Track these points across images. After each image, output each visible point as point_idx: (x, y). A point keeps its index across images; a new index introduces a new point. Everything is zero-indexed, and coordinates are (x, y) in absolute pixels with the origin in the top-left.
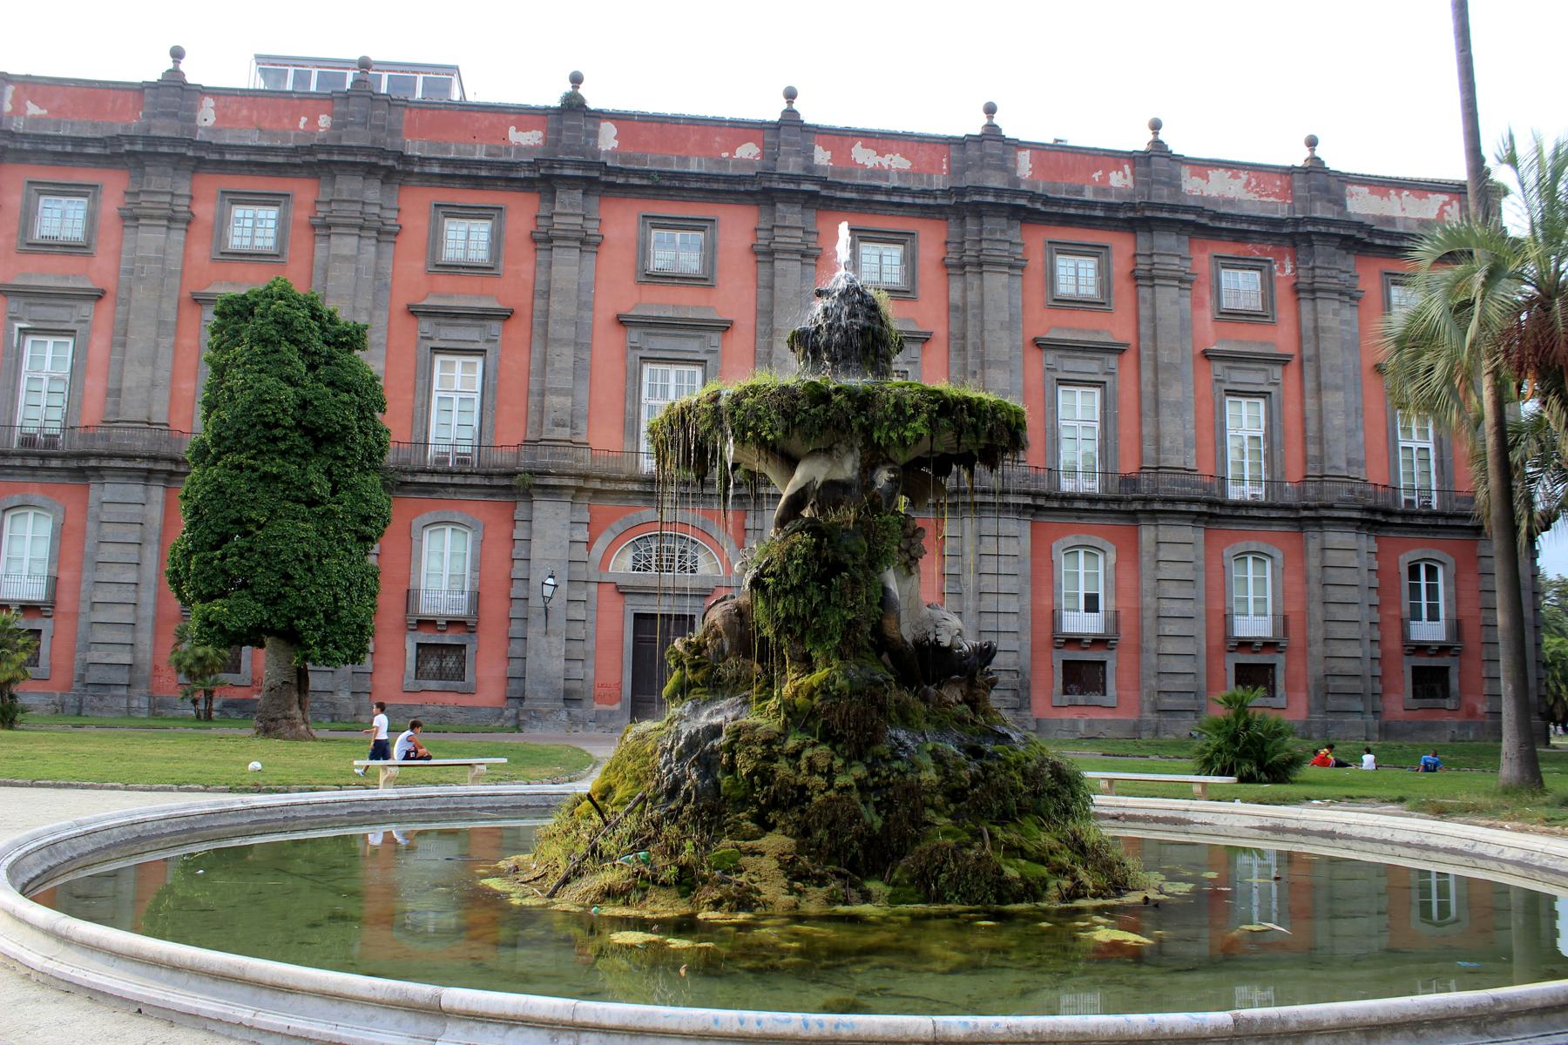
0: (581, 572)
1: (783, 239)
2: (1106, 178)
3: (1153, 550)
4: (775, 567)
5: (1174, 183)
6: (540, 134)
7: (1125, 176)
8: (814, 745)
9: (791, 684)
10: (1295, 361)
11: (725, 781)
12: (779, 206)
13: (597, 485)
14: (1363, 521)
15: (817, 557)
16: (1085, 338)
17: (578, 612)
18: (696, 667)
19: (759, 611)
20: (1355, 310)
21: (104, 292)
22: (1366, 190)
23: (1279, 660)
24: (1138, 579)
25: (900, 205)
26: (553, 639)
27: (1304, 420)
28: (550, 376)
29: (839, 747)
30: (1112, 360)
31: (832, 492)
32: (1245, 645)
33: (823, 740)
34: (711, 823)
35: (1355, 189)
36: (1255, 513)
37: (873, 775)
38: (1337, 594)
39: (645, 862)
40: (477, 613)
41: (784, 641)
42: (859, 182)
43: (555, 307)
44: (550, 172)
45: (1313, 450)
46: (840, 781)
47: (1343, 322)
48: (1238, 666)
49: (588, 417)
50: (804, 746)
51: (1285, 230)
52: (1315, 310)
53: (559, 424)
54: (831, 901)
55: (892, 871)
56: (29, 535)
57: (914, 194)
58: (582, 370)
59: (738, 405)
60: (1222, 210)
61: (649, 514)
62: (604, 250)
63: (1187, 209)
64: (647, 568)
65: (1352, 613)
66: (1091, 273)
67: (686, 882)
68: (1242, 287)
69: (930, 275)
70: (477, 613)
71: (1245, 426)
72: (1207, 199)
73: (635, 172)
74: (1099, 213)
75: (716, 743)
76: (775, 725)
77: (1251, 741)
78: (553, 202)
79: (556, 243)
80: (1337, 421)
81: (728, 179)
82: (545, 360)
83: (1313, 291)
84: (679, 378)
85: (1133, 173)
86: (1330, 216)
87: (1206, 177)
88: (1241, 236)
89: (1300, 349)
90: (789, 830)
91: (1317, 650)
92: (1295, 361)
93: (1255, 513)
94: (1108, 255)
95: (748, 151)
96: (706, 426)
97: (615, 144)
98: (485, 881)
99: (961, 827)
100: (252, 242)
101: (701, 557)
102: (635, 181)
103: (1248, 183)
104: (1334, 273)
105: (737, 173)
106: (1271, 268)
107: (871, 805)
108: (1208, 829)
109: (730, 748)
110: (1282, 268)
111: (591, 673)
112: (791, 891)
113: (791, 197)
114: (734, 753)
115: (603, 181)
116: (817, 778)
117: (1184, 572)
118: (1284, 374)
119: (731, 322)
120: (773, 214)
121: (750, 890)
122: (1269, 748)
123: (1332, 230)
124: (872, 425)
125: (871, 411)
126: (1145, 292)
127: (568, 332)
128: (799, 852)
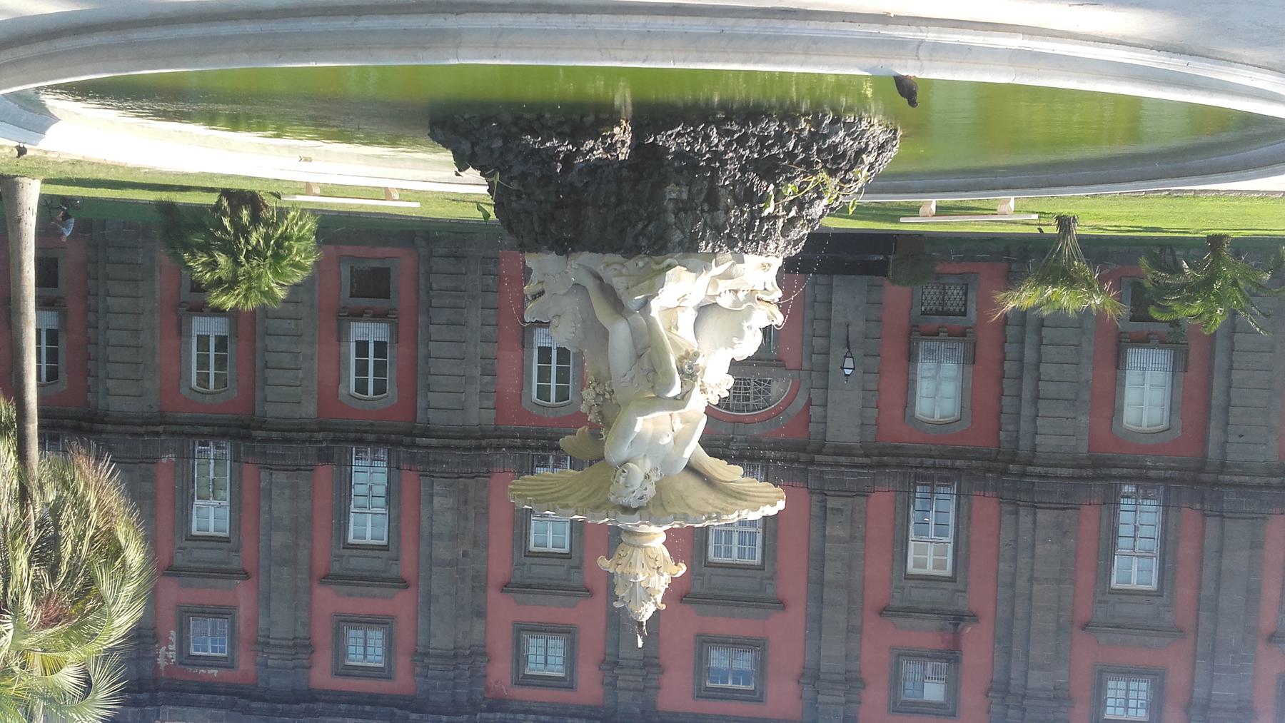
14: (102, 421)
16: (360, 588)
21: (1083, 629)
30: (336, 568)
32: (379, 316)
40: (910, 343)
53: (838, 511)
56: (1145, 407)
69: (501, 645)
70: (910, 343)
79: (291, 643)
84: (729, 552)
100: (1128, 686)
126: (301, 632)
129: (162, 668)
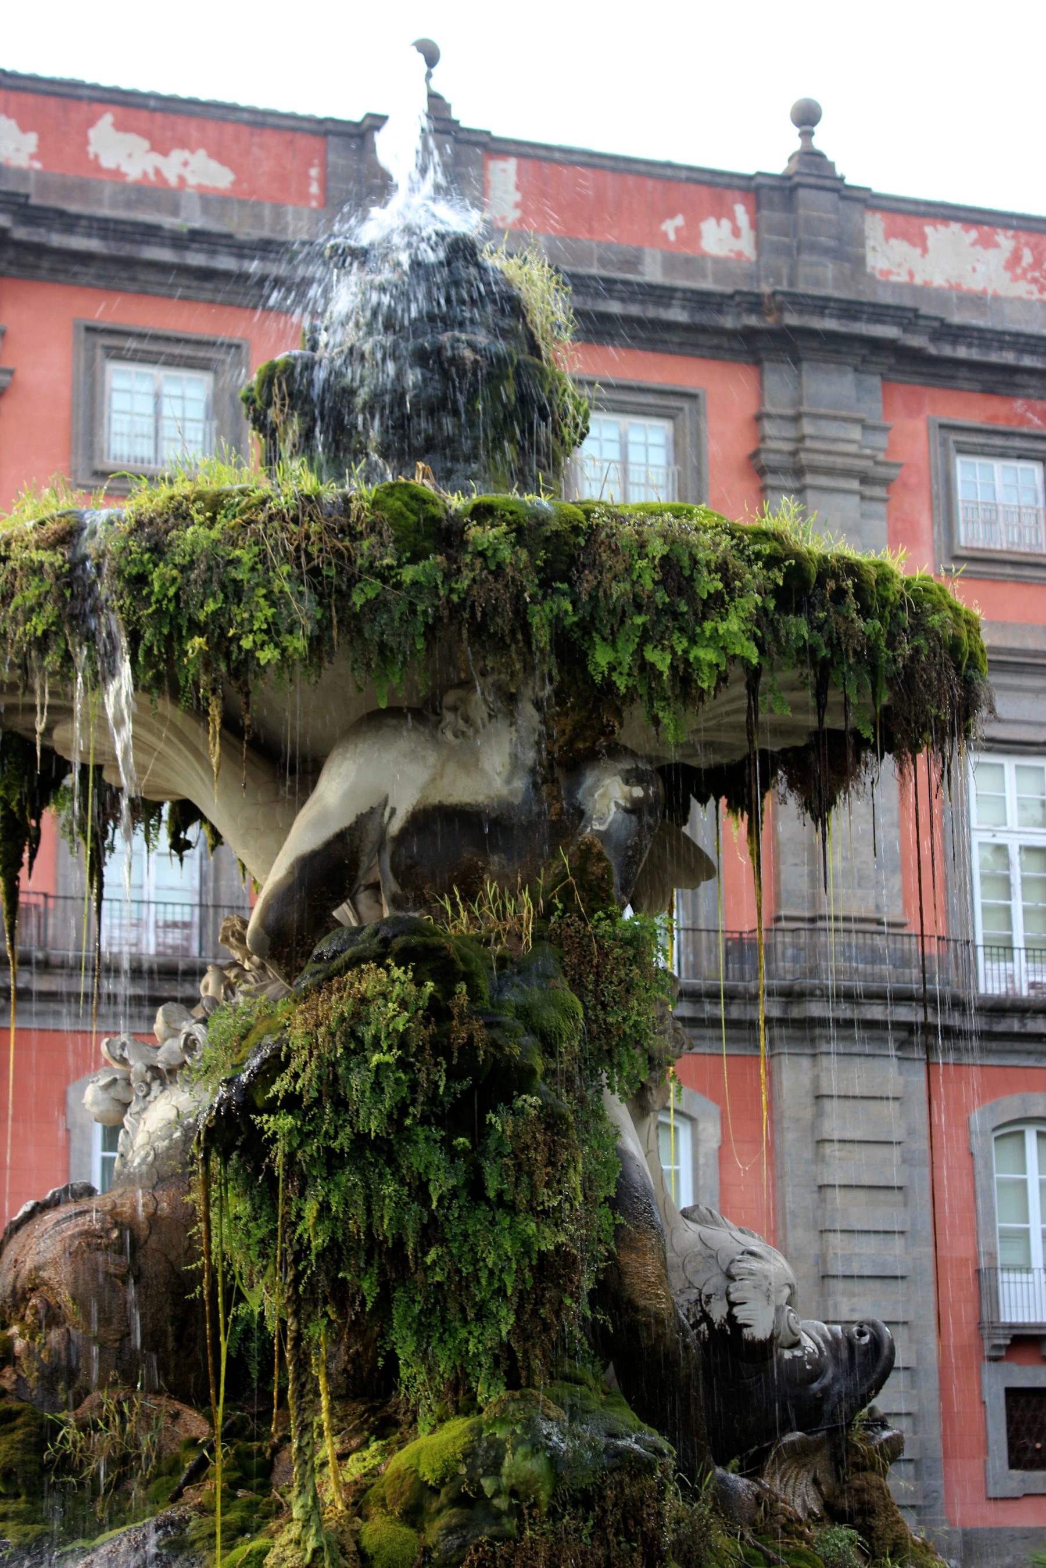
2: (691, 235)
3: (808, 1114)
4: (302, 1078)
5: (848, 252)
7: (736, 232)
15: (440, 1047)
19: (228, 1230)
24: (776, 1179)
25: (207, 275)
31: (447, 842)
41: (317, 1331)
42: (105, 211)
48: (1012, 1394)
59: (158, 550)
60: (957, 318)
63: (880, 313)
66: (659, 457)
68: (1003, 497)
72: (923, 291)
74: (677, 314)
85: (755, 225)
87: (920, 242)
88: (1000, 380)
94: (698, 413)
96: (39, 624)
103: (1015, 258)
124: (587, 627)
125: (588, 581)
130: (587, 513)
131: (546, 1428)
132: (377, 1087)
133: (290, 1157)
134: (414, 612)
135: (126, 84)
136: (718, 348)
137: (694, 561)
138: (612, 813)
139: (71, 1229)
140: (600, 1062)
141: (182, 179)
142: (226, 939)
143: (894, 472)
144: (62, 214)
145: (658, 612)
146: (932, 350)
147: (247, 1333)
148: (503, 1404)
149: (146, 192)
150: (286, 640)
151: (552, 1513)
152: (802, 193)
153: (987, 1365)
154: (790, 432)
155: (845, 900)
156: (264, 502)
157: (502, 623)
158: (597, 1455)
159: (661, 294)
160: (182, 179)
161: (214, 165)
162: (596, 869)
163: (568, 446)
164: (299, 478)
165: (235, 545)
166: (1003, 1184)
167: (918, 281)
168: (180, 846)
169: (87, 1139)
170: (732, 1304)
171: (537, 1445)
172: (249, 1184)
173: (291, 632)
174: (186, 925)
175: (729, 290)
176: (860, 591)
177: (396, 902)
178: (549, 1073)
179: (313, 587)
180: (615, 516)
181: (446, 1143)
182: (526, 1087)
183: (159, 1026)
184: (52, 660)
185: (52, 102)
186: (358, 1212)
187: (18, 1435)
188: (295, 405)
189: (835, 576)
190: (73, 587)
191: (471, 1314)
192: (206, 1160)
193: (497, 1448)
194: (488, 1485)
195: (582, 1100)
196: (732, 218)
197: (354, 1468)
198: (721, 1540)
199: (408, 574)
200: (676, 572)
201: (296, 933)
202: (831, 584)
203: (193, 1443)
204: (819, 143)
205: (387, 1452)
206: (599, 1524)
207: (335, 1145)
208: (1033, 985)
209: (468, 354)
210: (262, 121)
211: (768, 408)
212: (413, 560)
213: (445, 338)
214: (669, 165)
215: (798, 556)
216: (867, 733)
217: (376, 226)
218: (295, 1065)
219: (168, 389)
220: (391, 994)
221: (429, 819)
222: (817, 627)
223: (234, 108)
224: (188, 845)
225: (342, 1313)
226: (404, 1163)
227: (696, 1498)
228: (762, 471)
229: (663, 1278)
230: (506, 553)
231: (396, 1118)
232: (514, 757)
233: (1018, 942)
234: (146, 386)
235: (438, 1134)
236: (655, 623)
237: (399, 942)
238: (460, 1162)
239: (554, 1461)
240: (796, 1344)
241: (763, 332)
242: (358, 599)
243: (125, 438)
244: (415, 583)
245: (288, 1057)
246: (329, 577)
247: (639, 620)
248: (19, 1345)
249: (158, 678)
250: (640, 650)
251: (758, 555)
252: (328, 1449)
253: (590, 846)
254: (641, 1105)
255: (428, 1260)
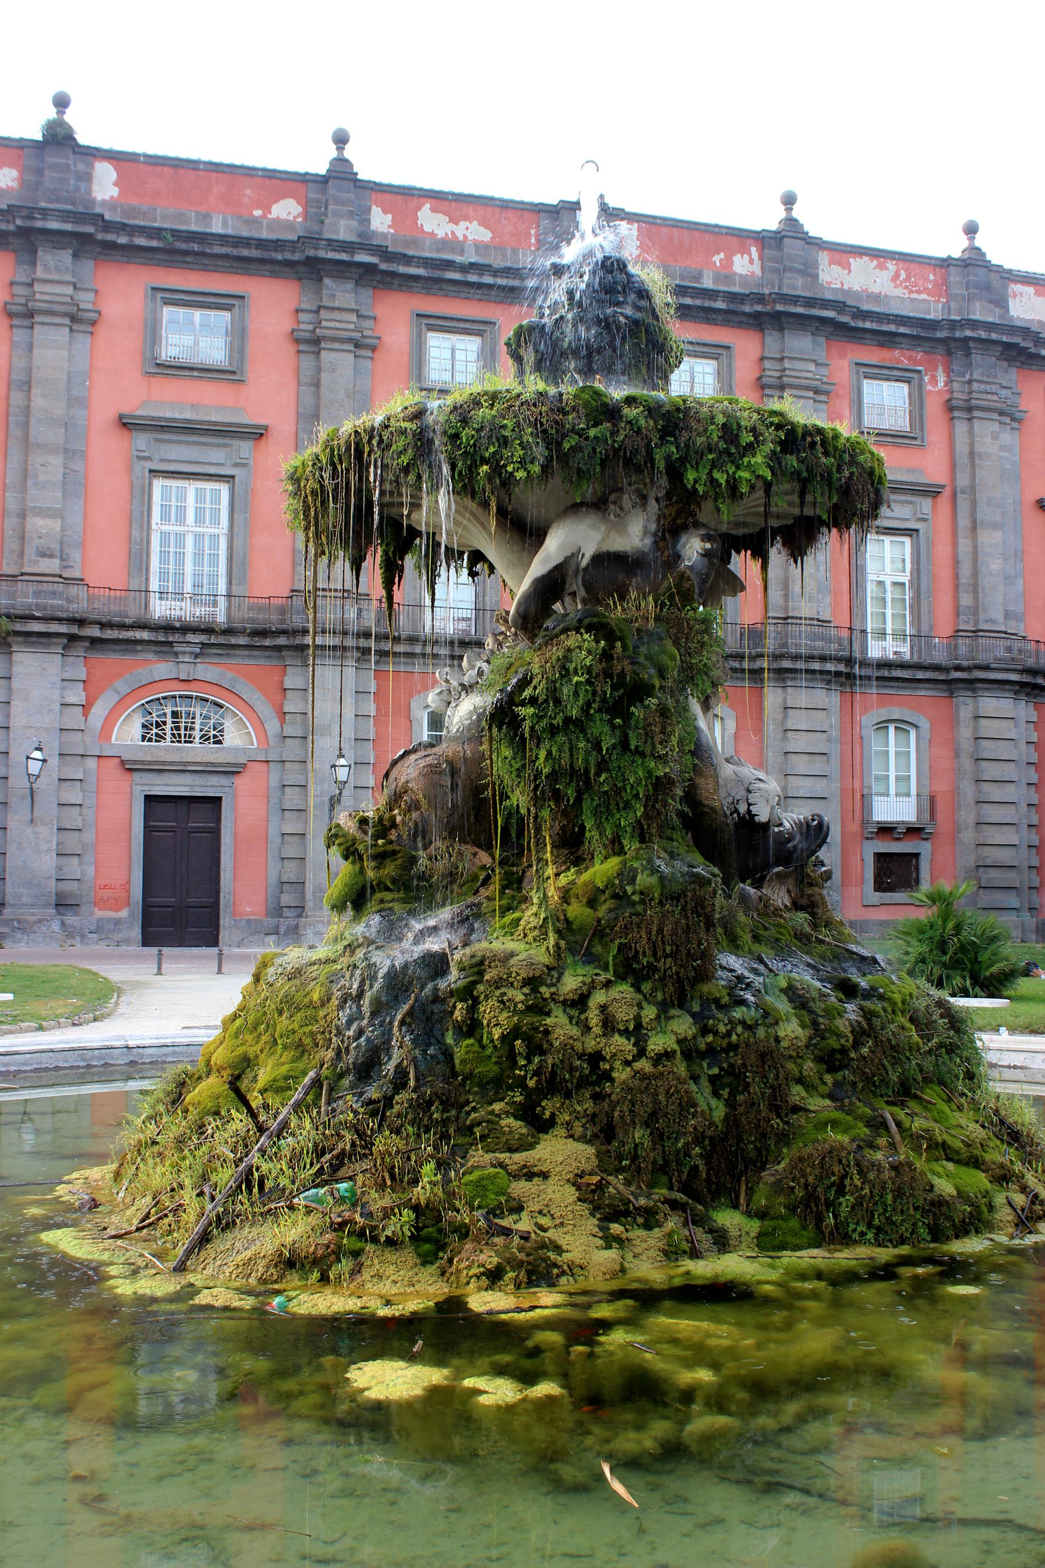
0: (76, 743)
1: (331, 323)
2: (728, 263)
3: (780, 717)
4: (538, 688)
5: (810, 271)
6: (14, 173)
7: (751, 261)
8: (608, 984)
9: (551, 881)
10: (946, 493)
11: (462, 1050)
12: (327, 281)
13: (95, 632)
14: (1022, 684)
15: (607, 674)
17: (73, 795)
18: (381, 857)
19: (501, 762)
20: (1016, 433)
22: (1031, 290)
23: (924, 848)
25: (480, 286)
26: (41, 829)
27: (956, 563)
28: (32, 492)
29: (646, 987)
31: (612, 570)
32: (886, 830)
33: (621, 977)
34: (445, 1122)
35: (1018, 288)
36: (898, 673)
37: (705, 1031)
38: (992, 771)
39: (355, 1201)
41: (545, 814)
42: (427, 254)
43: (38, 402)
44: (28, 224)
45: (966, 600)
46: (657, 1043)
47: (1002, 448)
48: (879, 857)
49: (83, 545)
50: (592, 986)
51: (938, 335)
52: (971, 432)
53: (45, 554)
54: (671, 1253)
55: (750, 1192)
57: (496, 272)
58: (74, 484)
59: (465, 421)
60: (865, 307)
61: (162, 669)
62: (101, 330)
63: (826, 304)
64: (160, 737)
65: (1008, 793)
66: (710, 379)
67: (432, 1237)
71: (888, 570)
72: (849, 292)
73: (143, 231)
74: (720, 305)
75: (442, 984)
76: (541, 955)
77: (963, 948)
78: (33, 264)
79: (38, 318)
80: (993, 565)
81: (262, 244)
82: (25, 474)
83: (970, 409)
84: (200, 497)
85: (761, 258)
86: (991, 320)
87: (847, 266)
88: (886, 340)
89: (953, 478)
90: (578, 1130)
91: (968, 836)
92: (946, 493)
93: (898, 673)
95: (287, 210)
96: (405, 459)
97: (115, 192)
98: (49, 1237)
99: (849, 1113)
101: (228, 724)
102: (141, 241)
103: (897, 275)
104: (994, 388)
105: (273, 236)
106: (921, 380)
107: (704, 1082)
108: (1018, 1075)
109: (467, 993)
110: (934, 380)
111: (90, 871)
112: (610, 1241)
113: (342, 270)
114: (476, 1001)
115: (99, 240)
116: (618, 1040)
117: (817, 743)
118: (934, 508)
119: (266, 428)
120: (318, 292)
121: (543, 1246)
122: (984, 957)
123: (994, 336)
124: (683, 460)
127: (55, 435)
128: (602, 1168)
129: (940, 369)
130: (684, 401)
131: (658, 862)
132: (576, 694)
133: (532, 728)
134: (595, 452)
135: (437, 187)
136: (741, 322)
137: (739, 426)
138: (695, 556)
139: (422, 763)
140: (687, 682)
141: (465, 236)
142: (497, 621)
143: (831, 388)
144: (404, 255)
145: (721, 453)
146: (853, 324)
147: (510, 815)
148: (638, 850)
149: (447, 243)
150: (530, 467)
151: (661, 903)
152: (786, 240)
153: (865, 842)
154: (777, 366)
155: (805, 609)
156: (518, 395)
157: (640, 458)
158: (683, 875)
159: (711, 294)
160: (465, 236)
161: (482, 229)
162: (686, 585)
163: (672, 368)
164: (535, 384)
165: (504, 418)
166: (877, 752)
167: (846, 287)
168: (472, 574)
169: (421, 726)
170: (749, 805)
171: (654, 871)
172: (511, 742)
173: (532, 463)
174: (469, 619)
175: (747, 292)
176: (824, 442)
177: (584, 601)
178: (662, 688)
179: (544, 440)
180: (698, 403)
181: (610, 722)
182: (650, 695)
183: (465, 663)
184: (411, 478)
185: (399, 197)
186: (566, 755)
187: (399, 862)
188: (536, 346)
189: (811, 435)
190: (422, 442)
191: (622, 805)
192: (490, 728)
193: (634, 872)
194: (629, 889)
195: (678, 701)
196: (750, 255)
197: (563, 880)
198: (742, 917)
199: (592, 432)
200: (730, 431)
201: (534, 617)
202: (809, 439)
203: (483, 867)
204: (795, 214)
205: (579, 873)
206: (684, 909)
207: (555, 722)
208: (895, 653)
209: (621, 319)
210: (506, 205)
211: (766, 354)
212: (595, 426)
213: (609, 311)
214: (717, 226)
215: (792, 424)
216: (825, 517)
217: (570, 254)
218: (534, 682)
219: (459, 346)
220: (583, 648)
221: (601, 559)
222: (801, 461)
223: (492, 199)
224: (477, 574)
225: (557, 804)
226: (589, 731)
227: (730, 897)
228: (763, 387)
229: (716, 791)
230: (642, 422)
231: (586, 709)
232: (645, 527)
233: (889, 631)
234: (447, 344)
235: (606, 717)
236: (719, 458)
237: (586, 621)
238: (617, 731)
239: (662, 878)
240: (781, 825)
241: (763, 314)
242: (566, 446)
243: (437, 371)
244: (596, 437)
245: (532, 679)
246: (552, 436)
247: (710, 457)
248: (399, 819)
249: (464, 487)
250: (710, 473)
251: (772, 424)
252: (550, 871)
253: (683, 574)
254: (706, 706)
255: (602, 779)
